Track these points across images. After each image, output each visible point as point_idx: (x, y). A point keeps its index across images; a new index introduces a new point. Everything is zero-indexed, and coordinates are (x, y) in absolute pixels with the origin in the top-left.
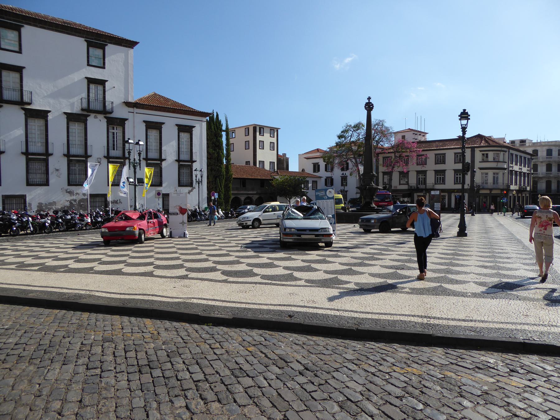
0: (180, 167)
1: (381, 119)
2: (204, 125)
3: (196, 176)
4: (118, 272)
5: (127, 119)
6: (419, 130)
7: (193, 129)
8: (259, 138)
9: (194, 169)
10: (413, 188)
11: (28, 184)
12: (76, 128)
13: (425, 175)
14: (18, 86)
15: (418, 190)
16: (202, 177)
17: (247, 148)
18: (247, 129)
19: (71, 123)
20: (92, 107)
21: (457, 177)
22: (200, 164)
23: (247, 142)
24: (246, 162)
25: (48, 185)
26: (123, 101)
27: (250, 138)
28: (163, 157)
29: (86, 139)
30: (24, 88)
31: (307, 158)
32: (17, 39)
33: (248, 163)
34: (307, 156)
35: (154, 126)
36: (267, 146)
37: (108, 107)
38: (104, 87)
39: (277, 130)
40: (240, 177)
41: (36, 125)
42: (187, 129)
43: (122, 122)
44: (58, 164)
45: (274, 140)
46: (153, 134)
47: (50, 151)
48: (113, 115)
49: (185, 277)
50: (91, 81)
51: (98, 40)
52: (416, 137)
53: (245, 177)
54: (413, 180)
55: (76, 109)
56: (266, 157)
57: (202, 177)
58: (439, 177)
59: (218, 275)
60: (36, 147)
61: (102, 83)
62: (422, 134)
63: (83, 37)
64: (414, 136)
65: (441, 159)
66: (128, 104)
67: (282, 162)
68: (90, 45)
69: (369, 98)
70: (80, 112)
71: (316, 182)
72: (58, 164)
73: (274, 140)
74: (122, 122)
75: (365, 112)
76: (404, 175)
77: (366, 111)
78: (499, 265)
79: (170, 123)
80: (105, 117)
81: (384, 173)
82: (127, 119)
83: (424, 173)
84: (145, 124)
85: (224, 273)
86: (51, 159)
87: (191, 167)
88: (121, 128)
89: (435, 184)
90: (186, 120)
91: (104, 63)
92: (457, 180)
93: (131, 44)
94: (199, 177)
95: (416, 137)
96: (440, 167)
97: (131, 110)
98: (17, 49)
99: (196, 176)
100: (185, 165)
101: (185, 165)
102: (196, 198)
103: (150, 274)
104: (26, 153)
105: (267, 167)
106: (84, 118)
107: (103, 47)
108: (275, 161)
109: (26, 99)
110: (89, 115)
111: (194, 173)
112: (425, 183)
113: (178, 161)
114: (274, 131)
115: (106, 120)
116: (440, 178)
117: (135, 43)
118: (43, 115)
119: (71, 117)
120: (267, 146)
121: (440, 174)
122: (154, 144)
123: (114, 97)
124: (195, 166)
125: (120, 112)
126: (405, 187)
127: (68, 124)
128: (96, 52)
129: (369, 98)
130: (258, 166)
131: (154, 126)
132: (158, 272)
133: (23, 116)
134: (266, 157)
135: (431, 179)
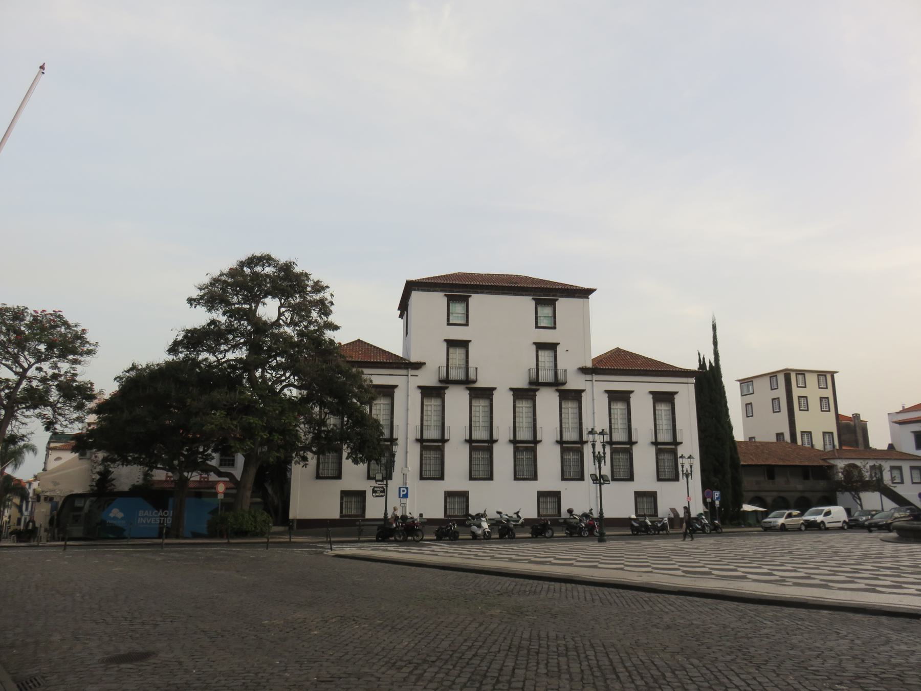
2: (692, 388)
3: (683, 466)
7: (676, 396)
8: (796, 392)
9: (679, 455)
11: (471, 478)
12: (432, 404)
14: (464, 362)
16: (691, 466)
17: (776, 410)
18: (773, 375)
19: (517, 402)
20: (542, 379)
23: (776, 400)
25: (559, 492)
27: (781, 393)
29: (535, 420)
30: (470, 365)
31: (901, 423)
32: (464, 311)
33: (780, 436)
34: (901, 420)
35: (620, 397)
36: (814, 403)
38: (556, 352)
39: (832, 374)
43: (575, 396)
44: (503, 456)
45: (828, 393)
46: (619, 407)
47: (495, 438)
51: (546, 294)
55: (522, 383)
57: (691, 466)
59: (679, 573)
61: (464, 344)
63: (441, 291)
66: (584, 370)
68: (451, 299)
70: (439, 385)
72: (503, 456)
73: (828, 393)
74: (575, 396)
78: (21, 387)
79: (641, 391)
80: (557, 390)
82: (583, 391)
84: (651, 396)
85: (684, 571)
86: (540, 448)
87: (674, 452)
90: (664, 385)
91: (555, 323)
93: (585, 293)
94: (687, 467)
97: (589, 377)
98: (463, 322)
99: (683, 466)
100: (666, 450)
101: (666, 450)
102: (685, 496)
105: (818, 444)
106: (532, 393)
108: (833, 428)
109: (472, 376)
111: (680, 461)
115: (558, 394)
117: (591, 291)
118: (487, 394)
119: (518, 394)
120: (814, 403)
122: (664, 422)
123: (569, 363)
124: (681, 451)
125: (575, 382)
130: (799, 442)
131: (620, 397)
132: (626, 568)
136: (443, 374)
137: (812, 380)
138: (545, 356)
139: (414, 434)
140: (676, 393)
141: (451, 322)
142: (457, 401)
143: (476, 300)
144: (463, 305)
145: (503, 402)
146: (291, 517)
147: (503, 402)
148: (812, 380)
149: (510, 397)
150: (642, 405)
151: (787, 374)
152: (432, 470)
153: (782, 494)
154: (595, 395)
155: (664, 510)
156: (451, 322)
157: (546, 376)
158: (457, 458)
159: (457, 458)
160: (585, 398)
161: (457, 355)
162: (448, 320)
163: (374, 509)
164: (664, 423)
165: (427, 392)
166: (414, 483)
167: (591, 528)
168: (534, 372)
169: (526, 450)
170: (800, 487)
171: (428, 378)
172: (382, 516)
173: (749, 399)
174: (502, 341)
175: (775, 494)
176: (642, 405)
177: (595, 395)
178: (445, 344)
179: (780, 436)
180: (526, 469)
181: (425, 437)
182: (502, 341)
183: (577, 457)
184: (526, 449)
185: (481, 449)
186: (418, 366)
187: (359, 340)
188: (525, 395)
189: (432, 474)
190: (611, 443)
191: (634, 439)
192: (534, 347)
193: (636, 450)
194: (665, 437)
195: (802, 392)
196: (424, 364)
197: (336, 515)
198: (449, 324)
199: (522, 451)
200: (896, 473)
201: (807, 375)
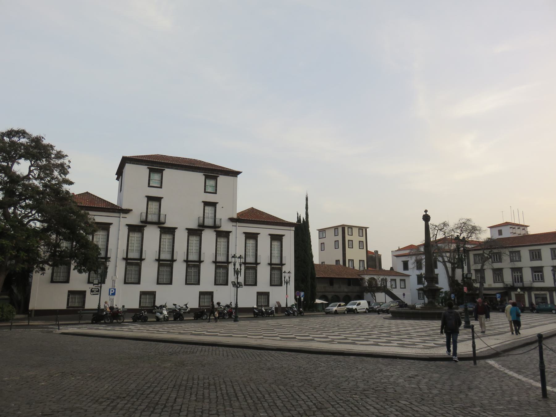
0: (272, 269)
1: (468, 218)
4: (231, 336)
5: (231, 232)
6: (517, 222)
8: (347, 238)
9: (283, 271)
10: (509, 286)
13: (521, 272)
15: (514, 288)
18: (336, 228)
20: (149, 219)
21: (535, 275)
22: (289, 267)
24: (336, 261)
26: (230, 217)
27: (340, 238)
28: (258, 262)
31: (397, 256)
33: (337, 261)
36: (356, 244)
37: (162, 219)
38: (216, 208)
40: (327, 276)
41: (167, 238)
42: (277, 238)
43: (226, 235)
45: (363, 239)
46: (251, 242)
48: (166, 225)
49: (263, 338)
50: (206, 204)
51: (212, 172)
52: (514, 231)
53: (332, 276)
54: (508, 278)
55: (194, 226)
56: (356, 256)
58: (537, 274)
59: (278, 338)
60: (193, 257)
61: (158, 200)
62: (522, 228)
63: (146, 165)
64: (511, 230)
65: (536, 255)
66: (232, 220)
67: (374, 260)
69: (426, 211)
70: (141, 224)
71: (404, 280)
73: (363, 239)
74: (226, 235)
75: (423, 223)
76: (498, 273)
77: (424, 222)
79: (264, 233)
81: (476, 271)
82: (231, 232)
83: (520, 270)
84: (244, 235)
85: (281, 337)
86: (202, 265)
87: (281, 269)
88: (225, 240)
89: (533, 282)
91: (216, 190)
92: (536, 277)
93: (235, 174)
94: (287, 278)
95: (514, 231)
96: (536, 264)
97: (234, 224)
101: (276, 268)
102: (284, 295)
103: (246, 337)
104: (159, 260)
105: (357, 267)
106: (200, 232)
107: (215, 178)
110: (203, 230)
111: (283, 274)
112: (522, 280)
113: (159, 260)
114: (363, 230)
116: (538, 275)
118: (171, 231)
119: (191, 232)
120: (356, 244)
121: (538, 271)
124: (284, 269)
125: (226, 226)
126: (500, 285)
127: (188, 237)
128: (211, 183)
129: (426, 211)
130: (347, 266)
133: (159, 232)
134: (356, 256)
135: (528, 277)
136: (201, 221)
137: (355, 231)
138: (209, 210)
139: (122, 254)
140: (259, 234)
141: (151, 185)
142: (152, 235)
143: (167, 172)
144: (160, 175)
145: (181, 237)
146: (30, 308)
147: (181, 237)
148: (355, 231)
149: (186, 233)
150: (264, 241)
151: (343, 227)
152: (133, 278)
153: (336, 294)
154: (238, 233)
155: (272, 303)
156: (151, 185)
157: (209, 222)
158: (149, 270)
159: (149, 270)
160: (231, 236)
161: (154, 206)
162: (149, 183)
163: (91, 303)
164: (276, 253)
165: (132, 228)
166: (120, 286)
167: (230, 314)
168: (201, 219)
169: (194, 266)
170: (346, 290)
171: (134, 219)
172: (96, 307)
173: (323, 240)
174: (182, 201)
175: (333, 294)
176: (264, 241)
177: (238, 233)
178: (146, 199)
179: (337, 261)
180: (193, 278)
181: (129, 257)
182: (182, 201)
183: (224, 271)
184: (194, 266)
185: (165, 265)
186: (127, 211)
187: (252, 208)
188: (195, 233)
189: (61, 279)
190: (245, 263)
191: (175, 258)
192: (203, 204)
193: (259, 268)
194: (276, 261)
195: (350, 238)
196: (131, 210)
197: (64, 306)
198: (149, 186)
199: (191, 267)
200: (393, 283)
201: (353, 228)
